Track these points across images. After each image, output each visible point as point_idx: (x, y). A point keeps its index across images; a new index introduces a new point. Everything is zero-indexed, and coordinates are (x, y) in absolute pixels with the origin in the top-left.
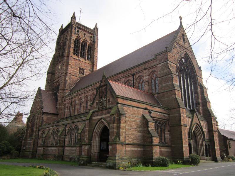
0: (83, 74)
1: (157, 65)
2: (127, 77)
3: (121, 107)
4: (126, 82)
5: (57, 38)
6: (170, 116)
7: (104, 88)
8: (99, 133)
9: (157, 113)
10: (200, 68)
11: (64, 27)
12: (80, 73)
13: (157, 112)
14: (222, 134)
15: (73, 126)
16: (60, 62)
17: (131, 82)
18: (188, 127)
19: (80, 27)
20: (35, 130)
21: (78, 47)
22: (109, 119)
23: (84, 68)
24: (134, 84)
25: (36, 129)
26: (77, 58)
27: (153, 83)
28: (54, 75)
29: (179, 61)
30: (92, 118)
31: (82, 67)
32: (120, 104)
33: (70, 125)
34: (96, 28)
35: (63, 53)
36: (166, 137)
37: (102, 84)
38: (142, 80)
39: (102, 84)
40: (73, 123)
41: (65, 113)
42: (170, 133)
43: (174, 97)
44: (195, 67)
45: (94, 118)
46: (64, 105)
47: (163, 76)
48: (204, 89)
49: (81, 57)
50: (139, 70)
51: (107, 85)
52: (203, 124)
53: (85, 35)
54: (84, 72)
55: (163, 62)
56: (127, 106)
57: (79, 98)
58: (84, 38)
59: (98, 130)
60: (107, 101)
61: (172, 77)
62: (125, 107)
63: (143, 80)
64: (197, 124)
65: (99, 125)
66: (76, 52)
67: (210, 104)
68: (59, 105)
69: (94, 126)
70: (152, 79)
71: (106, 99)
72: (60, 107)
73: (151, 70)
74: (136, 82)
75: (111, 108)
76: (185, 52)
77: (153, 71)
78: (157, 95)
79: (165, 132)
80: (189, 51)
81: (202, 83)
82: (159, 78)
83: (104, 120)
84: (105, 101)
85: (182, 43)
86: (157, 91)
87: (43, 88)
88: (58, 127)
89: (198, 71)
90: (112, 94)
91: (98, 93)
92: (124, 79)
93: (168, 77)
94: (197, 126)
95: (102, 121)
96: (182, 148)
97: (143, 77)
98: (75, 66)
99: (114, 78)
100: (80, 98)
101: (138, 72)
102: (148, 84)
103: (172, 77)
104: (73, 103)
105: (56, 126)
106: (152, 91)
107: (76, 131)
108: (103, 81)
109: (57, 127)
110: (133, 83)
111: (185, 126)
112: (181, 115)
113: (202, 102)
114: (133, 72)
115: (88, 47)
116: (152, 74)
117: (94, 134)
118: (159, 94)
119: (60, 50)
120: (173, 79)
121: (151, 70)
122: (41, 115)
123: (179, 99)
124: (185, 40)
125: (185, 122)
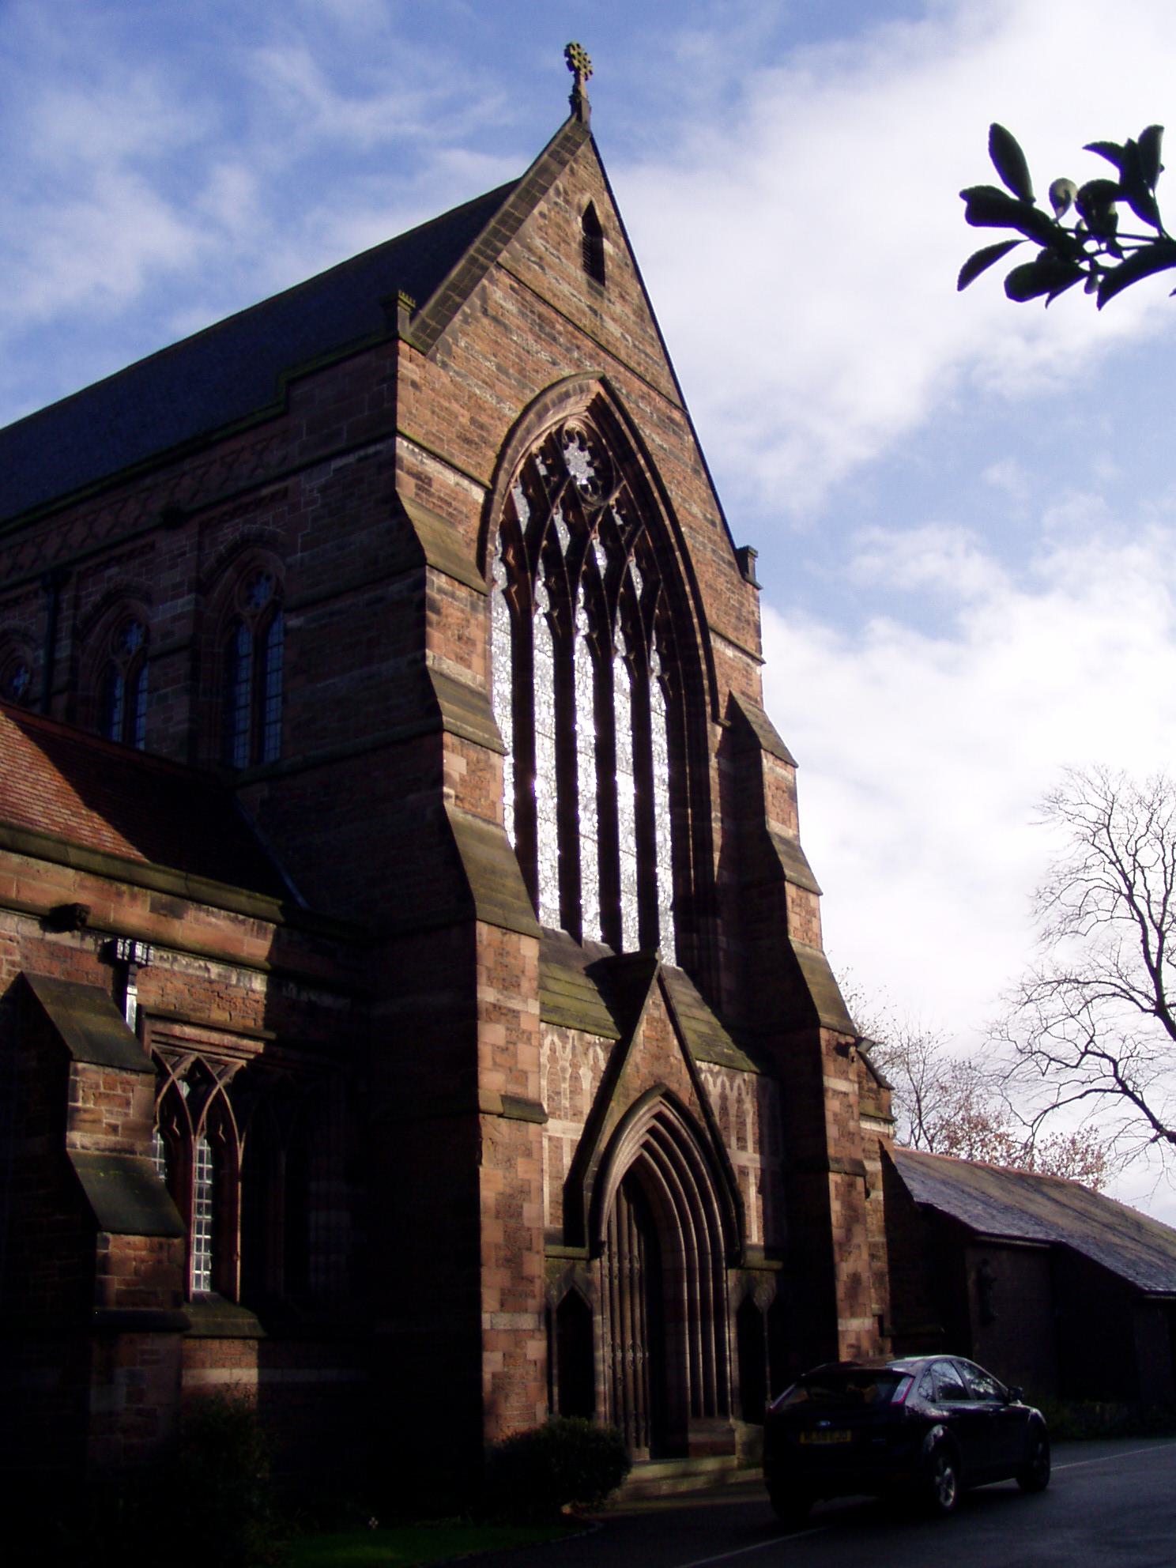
1: (289, 483)
9: (215, 969)
10: (743, 558)
13: (207, 969)
14: (920, 1192)
18: (565, 1131)
24: (61, 679)
27: (246, 671)
29: (530, 464)
44: (689, 542)
48: (767, 762)
52: (730, 1087)
63: (147, 639)
64: (670, 1097)
67: (813, 913)
73: (229, 533)
74: (74, 659)
76: (598, 388)
80: (641, 378)
81: (757, 702)
82: (297, 609)
85: (565, 288)
89: (721, 584)
94: (671, 1115)
96: (473, 1342)
111: (527, 1111)
112: (487, 994)
120: (432, 616)
124: (609, 267)
125: (522, 1077)
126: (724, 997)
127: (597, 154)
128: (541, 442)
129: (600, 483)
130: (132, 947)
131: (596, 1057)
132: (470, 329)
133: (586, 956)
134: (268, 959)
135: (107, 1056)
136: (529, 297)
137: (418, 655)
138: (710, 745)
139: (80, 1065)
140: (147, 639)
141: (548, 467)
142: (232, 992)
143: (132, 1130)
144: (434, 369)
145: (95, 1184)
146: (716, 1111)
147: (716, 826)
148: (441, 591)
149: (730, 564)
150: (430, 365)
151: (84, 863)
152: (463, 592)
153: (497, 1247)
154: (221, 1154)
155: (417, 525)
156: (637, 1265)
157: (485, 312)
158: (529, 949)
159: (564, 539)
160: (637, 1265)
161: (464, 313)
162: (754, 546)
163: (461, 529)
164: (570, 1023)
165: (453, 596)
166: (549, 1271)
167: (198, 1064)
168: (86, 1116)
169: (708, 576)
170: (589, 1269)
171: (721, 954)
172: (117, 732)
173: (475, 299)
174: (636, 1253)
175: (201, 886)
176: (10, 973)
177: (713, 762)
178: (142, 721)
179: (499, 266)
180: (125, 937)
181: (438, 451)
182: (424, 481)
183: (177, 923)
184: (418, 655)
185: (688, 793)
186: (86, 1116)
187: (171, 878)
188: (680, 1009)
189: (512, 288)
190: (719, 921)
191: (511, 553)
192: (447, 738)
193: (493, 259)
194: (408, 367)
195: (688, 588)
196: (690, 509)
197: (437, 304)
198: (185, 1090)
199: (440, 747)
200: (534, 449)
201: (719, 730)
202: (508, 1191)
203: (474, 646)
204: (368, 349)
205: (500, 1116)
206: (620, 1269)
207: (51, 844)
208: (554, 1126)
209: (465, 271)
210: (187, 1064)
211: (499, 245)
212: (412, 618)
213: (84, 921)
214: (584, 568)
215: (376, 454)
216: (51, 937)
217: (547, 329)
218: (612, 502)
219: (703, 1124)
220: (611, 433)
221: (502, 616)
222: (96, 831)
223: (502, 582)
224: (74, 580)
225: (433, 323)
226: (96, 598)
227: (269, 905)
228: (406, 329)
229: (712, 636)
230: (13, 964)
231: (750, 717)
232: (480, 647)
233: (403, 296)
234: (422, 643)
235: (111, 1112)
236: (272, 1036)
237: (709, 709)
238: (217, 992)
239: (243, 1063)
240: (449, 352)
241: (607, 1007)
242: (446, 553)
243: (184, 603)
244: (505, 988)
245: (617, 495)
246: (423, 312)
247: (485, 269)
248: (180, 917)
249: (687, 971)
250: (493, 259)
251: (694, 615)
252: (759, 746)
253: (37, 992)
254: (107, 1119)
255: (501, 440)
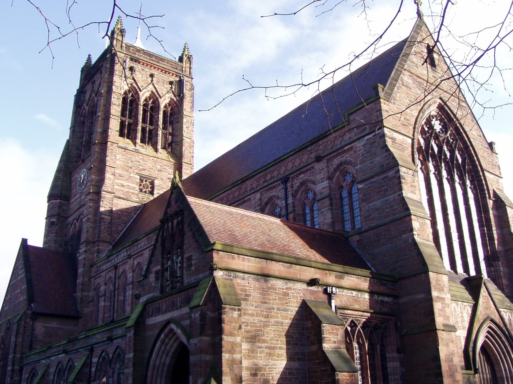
0: (152, 193)
1: (353, 145)
2: (268, 190)
3: (227, 279)
4: (267, 204)
5: (75, 93)
6: (401, 301)
7: (175, 221)
8: (166, 369)
9: (354, 293)
10: (491, 145)
11: (94, 61)
12: (141, 190)
13: (352, 293)
15: (111, 350)
16: (83, 161)
17: (279, 202)
18: (462, 334)
19: (136, 56)
20: (9, 368)
21: (133, 114)
22: (188, 322)
23: (154, 174)
24: (290, 209)
25: (13, 365)
26: (131, 146)
27: (346, 201)
28: (69, 201)
29: (423, 128)
30: (144, 322)
31: (146, 173)
32: (221, 269)
33: (103, 348)
34: (185, 58)
35: (91, 134)
36: (389, 370)
37: (168, 210)
38: (311, 195)
39: (168, 210)
40: (111, 339)
41: (100, 313)
42: (402, 356)
43: (410, 241)
44: (474, 143)
45: (152, 321)
46: (95, 289)
47: (373, 177)
49: (143, 141)
50: (302, 165)
51: (183, 214)
53: (154, 79)
54: (153, 188)
55: (367, 131)
56: (246, 276)
57: (136, 263)
58: (151, 87)
59: (163, 361)
60: (185, 265)
61: (397, 175)
62: (239, 281)
63: (315, 194)
64: (492, 321)
65: (163, 341)
66: (127, 131)
68: (82, 290)
69: (149, 345)
70: (342, 187)
71: (182, 258)
72: (84, 294)
73: (336, 162)
74: (293, 203)
75: (195, 286)
77: (341, 164)
78: (357, 238)
79: (388, 355)
82: (360, 182)
83: (178, 327)
84: (179, 265)
86: (357, 227)
87: (37, 240)
88: (72, 356)
89: (485, 155)
90: (197, 241)
91: (160, 239)
92: (258, 195)
93: (386, 177)
94: (494, 326)
95: (172, 330)
97: (314, 183)
98: (127, 171)
99: (231, 196)
100: (139, 264)
101: (300, 171)
102: (331, 205)
103: (397, 175)
104: (121, 281)
105: (65, 352)
106: (344, 227)
107: (118, 366)
108: (173, 203)
109: (69, 356)
110: (287, 204)
111: (451, 329)
112: (435, 294)
113: (506, 251)
114: (282, 170)
115: (164, 112)
116: (341, 172)
117: (149, 374)
118: (363, 232)
119: (84, 128)
120: (402, 180)
121: (336, 162)
122: (28, 320)
123: (427, 246)
124: (437, 62)
125: (448, 318)
126: (505, 287)
127: (427, 28)
128: (425, 121)
129: (444, 130)
130: (332, 288)
131: (468, 310)
132: (399, 91)
133: (459, 278)
134: (369, 288)
135: (331, 322)
136: (415, 77)
137: (400, 193)
138: (489, 206)
139: (324, 325)
140: (315, 194)
141: (428, 128)
142: (360, 299)
143: (339, 342)
144: (391, 105)
145: (333, 358)
146: (508, 324)
147: (495, 232)
148: (404, 172)
149: (487, 148)
150: (390, 104)
151: (316, 266)
152: (411, 172)
153: (447, 371)
154: (361, 347)
155: (394, 153)
156: (488, 376)
157: (403, 85)
158: (445, 278)
159: (436, 149)
160: (488, 376)
161: (397, 87)
162: (493, 141)
163: (406, 152)
164: (459, 300)
165: (408, 173)
166: (463, 378)
167: (352, 321)
168: (327, 339)
169: (481, 153)
170: (474, 377)
171: (502, 273)
172: (309, 224)
173: (400, 81)
174: (487, 372)
175: (348, 269)
176: (300, 299)
177: (491, 212)
178: (316, 220)
179: (405, 70)
180: (330, 286)
181: (396, 130)
182: (393, 139)
183: (342, 280)
184: (400, 193)
185: (484, 223)
186: (327, 339)
187: (339, 268)
188: (492, 292)
189: (410, 75)
190: (500, 263)
191: (421, 156)
192: (413, 217)
193: (403, 68)
194: (384, 106)
195: (475, 158)
196: (473, 134)
197: (389, 85)
198: (349, 329)
199: (411, 220)
200: (423, 123)
201: (491, 202)
202: (448, 354)
203: (414, 188)
204: (371, 102)
205: (443, 330)
206: (483, 377)
207: (292, 259)
208: (458, 333)
209: (395, 73)
210: (349, 322)
211: (404, 63)
212: (397, 182)
213: (318, 283)
214: (443, 157)
215: (379, 133)
216: (310, 288)
217: (422, 86)
218: (448, 135)
219: (504, 329)
220: (445, 114)
221: (421, 176)
222: (314, 255)
223: (420, 166)
224: (290, 179)
225: (389, 91)
226: (298, 184)
227: (367, 272)
228: (382, 94)
229: (485, 172)
230: (301, 297)
231: (501, 196)
232: (417, 187)
233: (379, 85)
234: (401, 189)
235: (333, 337)
236: (372, 311)
237: (487, 195)
238: (356, 300)
239: (365, 320)
240: (395, 99)
241: (469, 294)
242: (405, 161)
243: (325, 184)
244: (440, 291)
245: (449, 132)
246: (386, 89)
247: (401, 72)
248: (343, 279)
249: (491, 280)
250: (403, 68)
251: (479, 166)
252: (505, 205)
253: (309, 304)
254: (333, 340)
255: (414, 123)
